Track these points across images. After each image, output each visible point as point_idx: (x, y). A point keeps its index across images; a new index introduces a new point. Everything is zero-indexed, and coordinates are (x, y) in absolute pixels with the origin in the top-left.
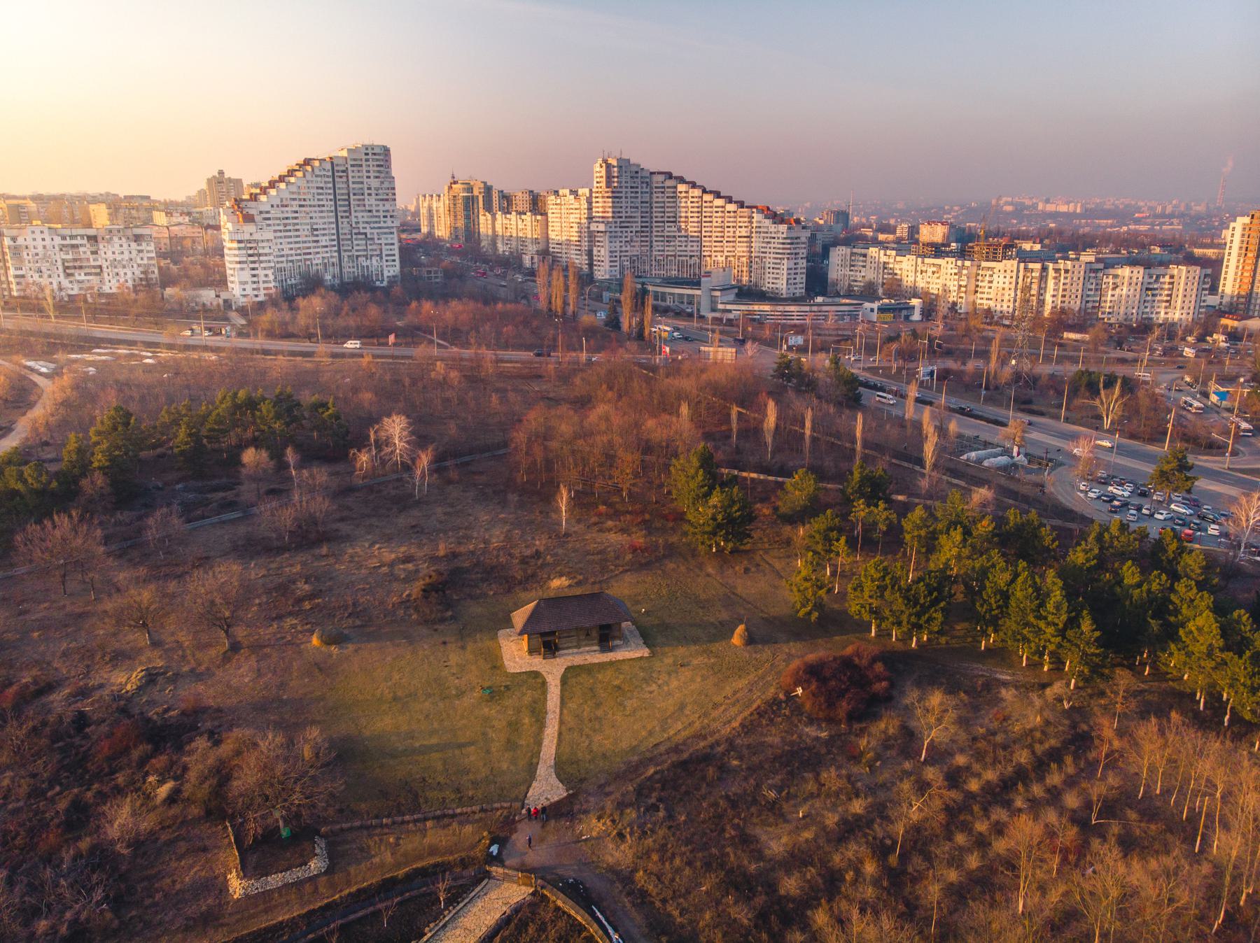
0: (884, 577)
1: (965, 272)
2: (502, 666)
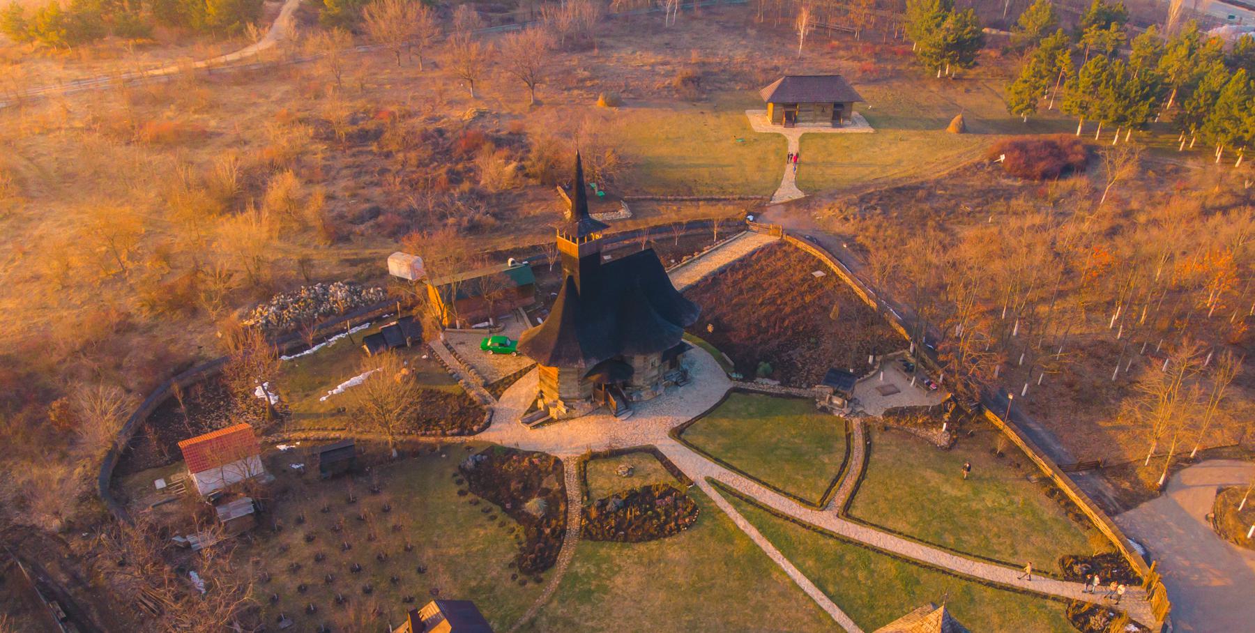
0: (1100, 73)
2: (751, 128)
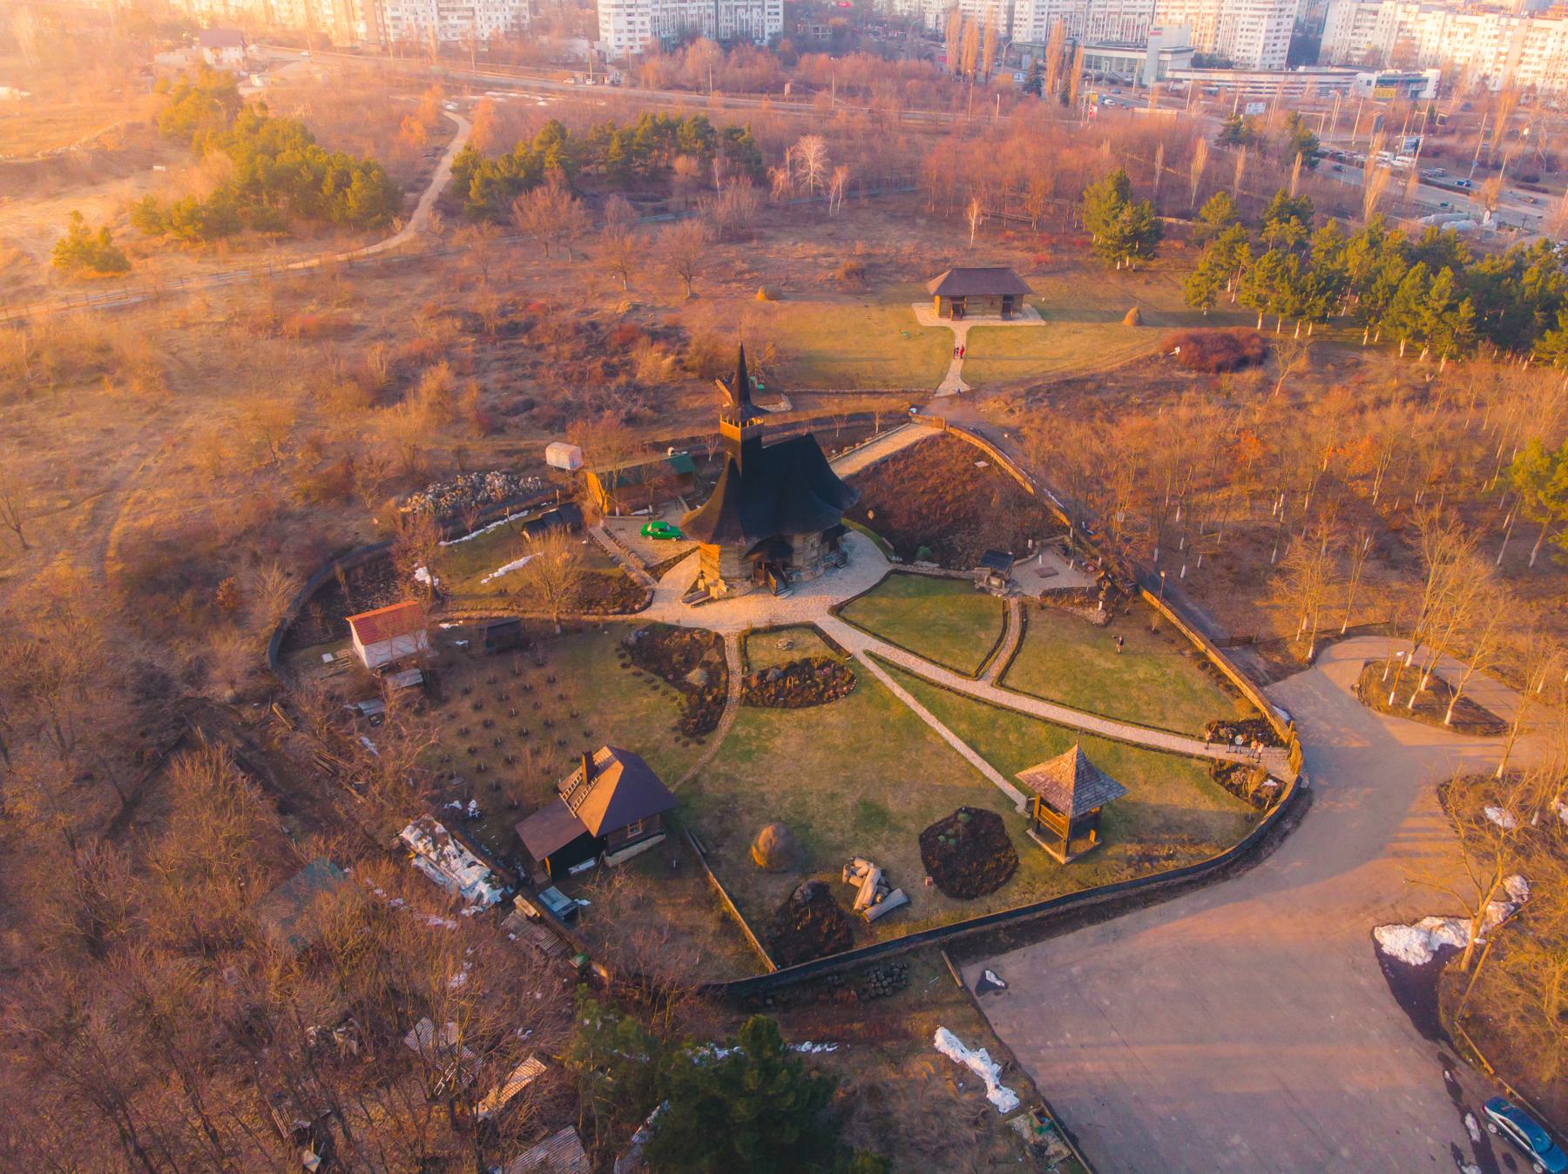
1: (1509, 34)
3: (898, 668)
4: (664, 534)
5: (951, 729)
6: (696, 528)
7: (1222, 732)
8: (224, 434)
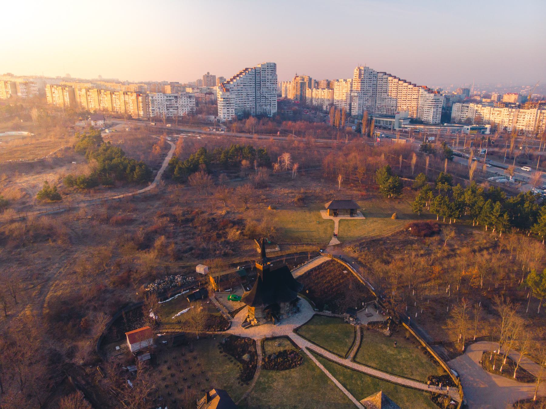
1: (512, 114)
3: (318, 354)
4: (235, 299)
5: (337, 379)
6: (247, 300)
7: (434, 380)
8: (87, 260)
